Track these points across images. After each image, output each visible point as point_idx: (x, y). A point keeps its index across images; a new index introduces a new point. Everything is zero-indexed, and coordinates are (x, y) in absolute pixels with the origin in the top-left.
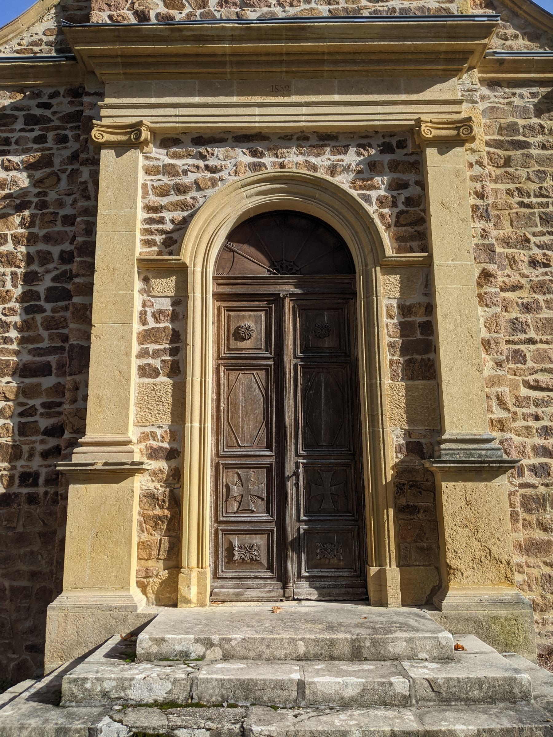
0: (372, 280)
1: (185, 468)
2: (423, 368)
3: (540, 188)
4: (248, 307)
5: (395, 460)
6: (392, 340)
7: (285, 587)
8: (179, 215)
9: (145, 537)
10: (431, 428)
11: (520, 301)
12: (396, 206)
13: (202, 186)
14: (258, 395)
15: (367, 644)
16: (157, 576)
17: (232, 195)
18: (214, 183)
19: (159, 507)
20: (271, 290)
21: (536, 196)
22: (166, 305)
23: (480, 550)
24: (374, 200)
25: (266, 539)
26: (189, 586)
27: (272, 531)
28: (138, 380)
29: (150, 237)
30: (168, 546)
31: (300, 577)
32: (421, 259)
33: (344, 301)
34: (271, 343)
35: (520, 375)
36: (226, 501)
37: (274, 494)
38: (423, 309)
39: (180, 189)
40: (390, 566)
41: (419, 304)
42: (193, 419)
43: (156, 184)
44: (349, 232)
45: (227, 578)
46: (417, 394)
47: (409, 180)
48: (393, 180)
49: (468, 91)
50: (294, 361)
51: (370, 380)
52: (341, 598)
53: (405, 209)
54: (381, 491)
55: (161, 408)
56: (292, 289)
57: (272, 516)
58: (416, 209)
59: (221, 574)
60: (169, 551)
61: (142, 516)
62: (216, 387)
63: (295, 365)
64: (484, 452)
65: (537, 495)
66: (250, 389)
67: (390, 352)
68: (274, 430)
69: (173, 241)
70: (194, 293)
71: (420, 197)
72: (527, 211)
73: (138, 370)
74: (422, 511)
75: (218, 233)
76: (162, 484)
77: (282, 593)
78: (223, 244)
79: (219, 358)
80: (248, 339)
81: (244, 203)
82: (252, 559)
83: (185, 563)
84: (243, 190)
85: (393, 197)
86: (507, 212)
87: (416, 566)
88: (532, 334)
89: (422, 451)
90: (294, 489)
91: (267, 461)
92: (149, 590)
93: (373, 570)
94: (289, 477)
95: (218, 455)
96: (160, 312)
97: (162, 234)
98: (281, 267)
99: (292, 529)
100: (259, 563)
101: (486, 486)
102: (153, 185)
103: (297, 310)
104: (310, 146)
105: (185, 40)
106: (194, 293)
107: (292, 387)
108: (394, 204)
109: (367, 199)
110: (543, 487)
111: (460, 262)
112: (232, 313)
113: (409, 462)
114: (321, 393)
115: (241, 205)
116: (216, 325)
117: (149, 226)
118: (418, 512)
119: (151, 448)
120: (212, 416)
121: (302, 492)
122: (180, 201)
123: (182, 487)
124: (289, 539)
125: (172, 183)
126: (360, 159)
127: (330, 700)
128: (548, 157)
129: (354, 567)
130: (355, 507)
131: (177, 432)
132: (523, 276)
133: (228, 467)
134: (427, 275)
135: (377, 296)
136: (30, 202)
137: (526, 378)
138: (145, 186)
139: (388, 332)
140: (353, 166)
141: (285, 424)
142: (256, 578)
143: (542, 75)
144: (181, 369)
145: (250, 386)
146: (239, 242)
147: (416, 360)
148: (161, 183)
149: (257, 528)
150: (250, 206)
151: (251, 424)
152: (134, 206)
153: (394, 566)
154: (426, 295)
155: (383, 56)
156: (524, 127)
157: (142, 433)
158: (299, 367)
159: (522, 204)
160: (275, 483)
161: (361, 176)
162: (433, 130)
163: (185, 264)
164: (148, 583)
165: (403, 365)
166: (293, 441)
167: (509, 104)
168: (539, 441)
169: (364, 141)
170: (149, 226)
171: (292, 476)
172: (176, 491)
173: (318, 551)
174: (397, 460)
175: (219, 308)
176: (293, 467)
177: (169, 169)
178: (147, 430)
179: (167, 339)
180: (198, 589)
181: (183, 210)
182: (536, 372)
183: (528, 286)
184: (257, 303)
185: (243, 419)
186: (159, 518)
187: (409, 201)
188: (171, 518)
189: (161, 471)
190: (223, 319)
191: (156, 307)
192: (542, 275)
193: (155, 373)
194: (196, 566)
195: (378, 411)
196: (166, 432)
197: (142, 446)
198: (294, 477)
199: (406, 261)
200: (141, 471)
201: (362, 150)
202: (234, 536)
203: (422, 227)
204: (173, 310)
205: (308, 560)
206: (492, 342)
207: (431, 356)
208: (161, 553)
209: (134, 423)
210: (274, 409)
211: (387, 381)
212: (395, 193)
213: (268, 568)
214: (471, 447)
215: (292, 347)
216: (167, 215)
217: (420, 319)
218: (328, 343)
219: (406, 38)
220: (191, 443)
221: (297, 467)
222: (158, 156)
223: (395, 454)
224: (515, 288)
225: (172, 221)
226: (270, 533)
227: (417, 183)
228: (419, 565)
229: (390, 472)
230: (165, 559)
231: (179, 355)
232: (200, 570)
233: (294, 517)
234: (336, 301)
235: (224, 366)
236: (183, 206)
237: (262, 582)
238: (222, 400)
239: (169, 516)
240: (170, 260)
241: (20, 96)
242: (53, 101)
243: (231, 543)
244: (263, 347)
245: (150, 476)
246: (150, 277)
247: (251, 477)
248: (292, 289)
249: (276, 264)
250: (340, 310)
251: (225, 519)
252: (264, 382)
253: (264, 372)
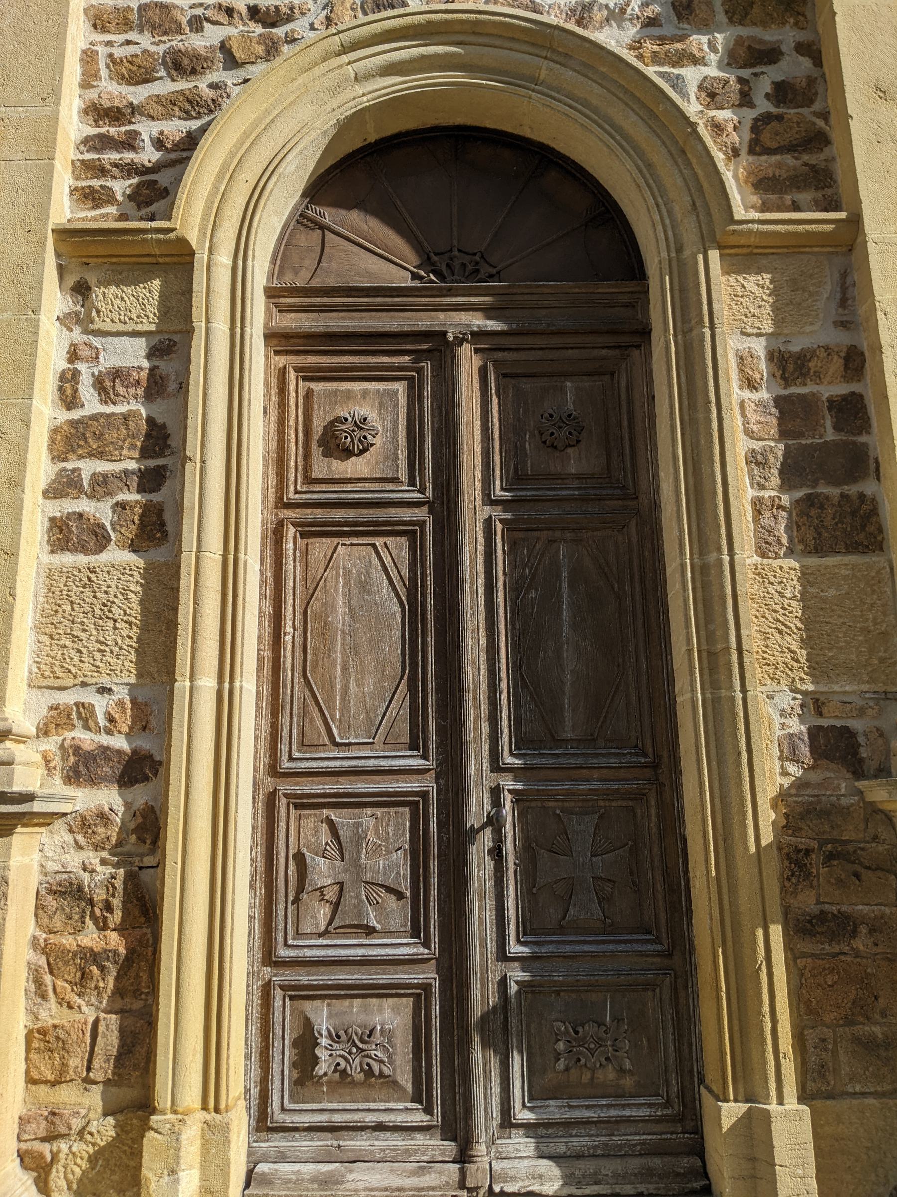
0: (698, 285)
1: (172, 810)
2: (848, 519)
4: (362, 369)
5: (780, 780)
6: (757, 446)
7: (464, 1157)
8: (176, 128)
9: (51, 1014)
10: (879, 687)
12: (751, 105)
13: (239, 55)
14: (388, 602)
16: (81, 1133)
17: (317, 71)
18: (271, 50)
19: (96, 924)
20: (423, 322)
22: (132, 354)
24: (692, 90)
25: (409, 1010)
26: (173, 1172)
27: (426, 987)
28: (46, 558)
29: (96, 183)
30: (116, 1042)
31: (507, 1122)
32: (829, 228)
33: (617, 352)
34: (422, 464)
36: (297, 900)
37: (434, 880)
38: (837, 364)
39: (182, 65)
40: (781, 1102)
41: (827, 348)
42: (199, 666)
43: (118, 53)
44: (629, 164)
45: (296, 1129)
46: (832, 592)
47: (781, 42)
48: (739, 41)
50: (485, 512)
51: (701, 554)
53: (773, 109)
54: (745, 874)
55: (110, 636)
57: (426, 944)
58: (805, 111)
59: (280, 1117)
60: (118, 1058)
61: (44, 952)
62: (271, 581)
63: (489, 523)
66: (365, 587)
67: (752, 478)
68: (432, 697)
69: (155, 191)
70: (208, 320)
71: (811, 81)
73: (50, 529)
74: (863, 929)
75: (280, 169)
76: (105, 854)
77: (456, 1177)
78: (295, 209)
79: (282, 503)
80: (362, 452)
81: (348, 94)
82: (369, 1073)
83: (163, 1096)
84: (345, 58)
85: (740, 80)
87: (854, 1094)
89: (855, 753)
90: (490, 864)
91: (412, 785)
92: (57, 1179)
93: (731, 1112)
94: (475, 831)
95: (273, 770)
96: (116, 373)
97: (129, 176)
98: (447, 264)
99: (485, 981)
100: (390, 1083)
102: (111, 56)
103: (492, 376)
106: (208, 320)
107: (481, 582)
108: (745, 99)
109: (677, 83)
112: (317, 386)
113: (819, 785)
114: (559, 596)
115: (341, 99)
116: (273, 416)
117: (96, 156)
118: (854, 933)
119: (77, 750)
120: (260, 660)
121: (511, 873)
122: (182, 92)
123: (160, 866)
124: (477, 1011)
125: (162, 49)
129: (663, 1091)
130: (662, 916)
131: (152, 709)
133: (301, 803)
134: (844, 275)
135: (712, 327)
138: (88, 57)
139: (746, 423)
141: (461, 681)
142: (380, 1127)
144: (170, 528)
145: (365, 578)
146: (338, 204)
147: (827, 498)
148: (132, 50)
149: (383, 977)
150: (365, 102)
151: (369, 681)
152: (52, 95)
153: (792, 1103)
154: (843, 325)
157: (51, 708)
158: (499, 526)
160: (434, 850)
161: (656, 31)
163: (183, 242)
164: (55, 1156)
165: (790, 514)
166: (485, 727)
170: (96, 156)
171: (482, 828)
172: (145, 876)
173: (561, 1046)
174: (786, 782)
175: (282, 372)
176: (487, 801)
177: (155, 16)
178: (68, 698)
179: (132, 447)
180: (204, 1178)
181: (188, 117)
184: (385, 359)
185: (345, 668)
186: (94, 957)
187: (782, 92)
188: (127, 958)
189: (103, 818)
190: (292, 401)
191: (106, 362)
193: (98, 539)
194: (198, 1104)
195: (727, 640)
196: (120, 704)
197: (51, 744)
198: (488, 831)
199: (789, 234)
200: (47, 819)
202: (318, 1003)
203: (822, 156)
204: (152, 370)
205: (532, 1072)
207: (868, 487)
208: (96, 1064)
209: (30, 680)
210: (431, 640)
211: (747, 556)
212: (746, 73)
213: (416, 1099)
215: (478, 474)
216: (146, 129)
217: (831, 388)
218: (575, 462)
220: (190, 736)
221: (497, 803)
223: (778, 763)
225: (159, 143)
226: (420, 995)
227: (803, 49)
228: (863, 1094)
229: (768, 817)
230: (107, 1083)
231: (165, 490)
232: (210, 1116)
233: (491, 946)
234: (595, 352)
235: (294, 525)
236: (192, 106)
237: (396, 1141)
238: (289, 616)
239: (122, 950)
240: (145, 231)
243: (308, 1024)
245: (71, 831)
246: (92, 280)
247: (366, 831)
248: (478, 321)
249: (435, 258)
250: (607, 378)
251: (292, 953)
252: (405, 570)
253: (403, 541)
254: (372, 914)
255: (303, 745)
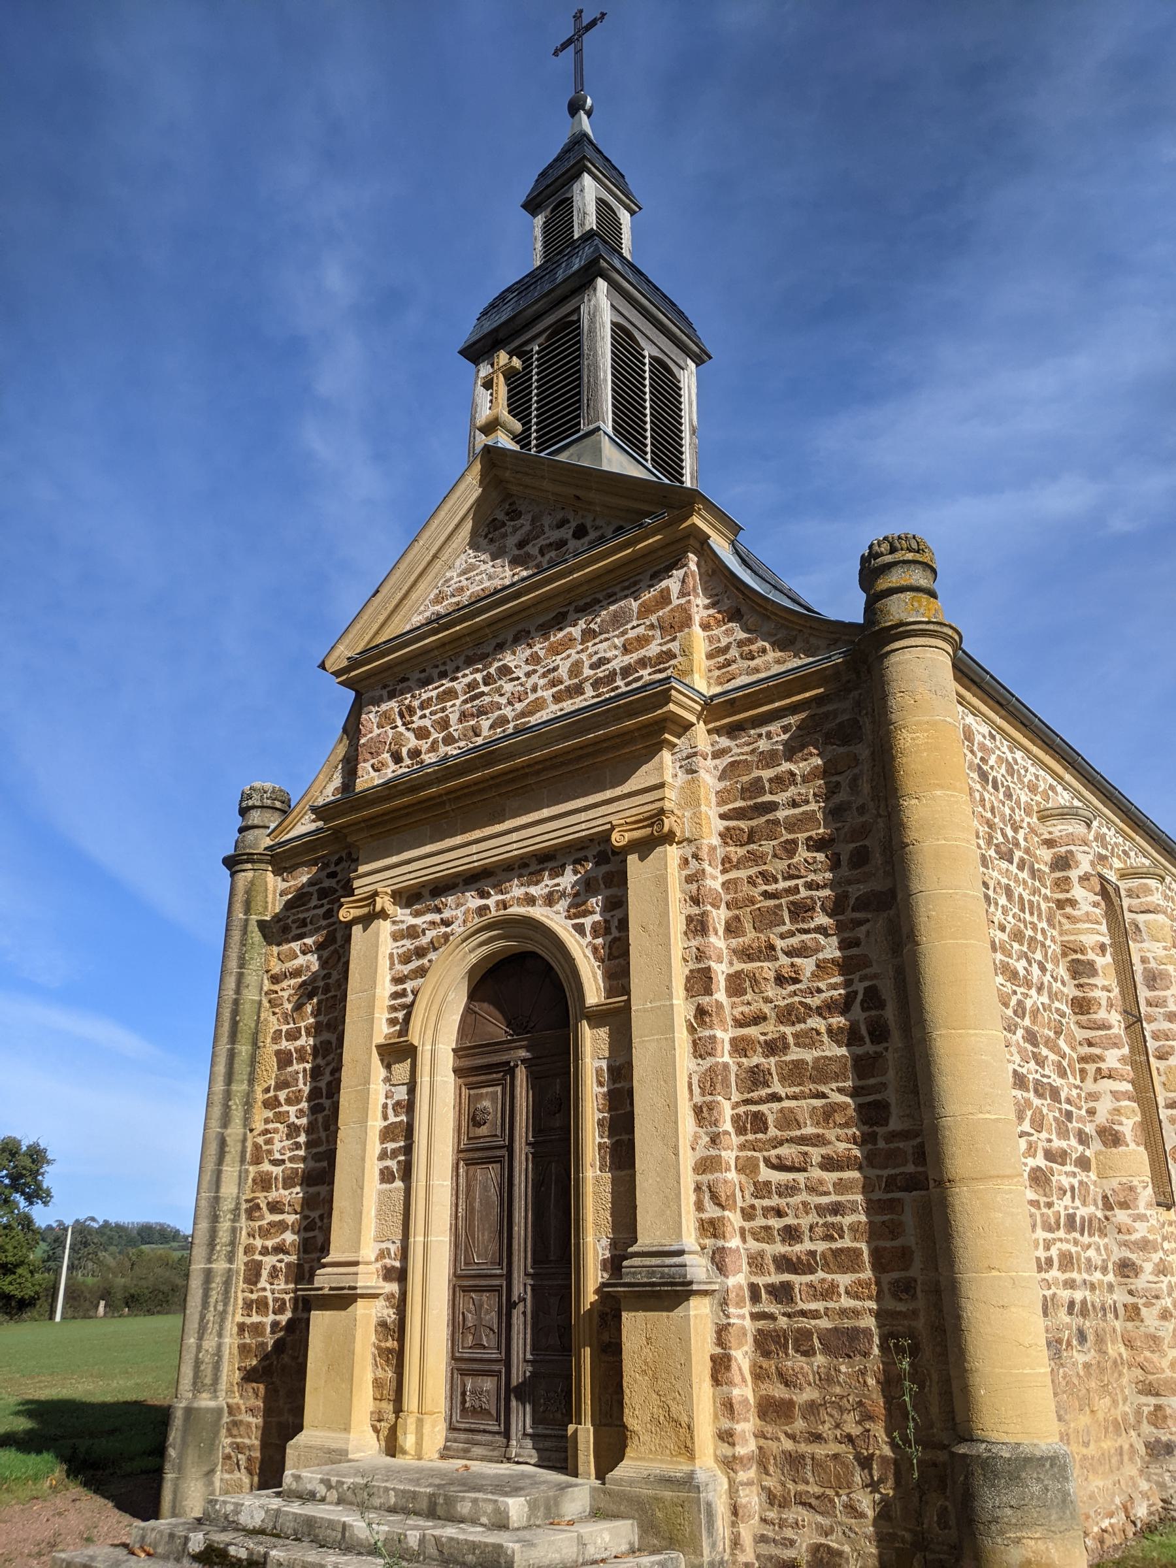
3: (789, 866)
9: (380, 1373)
11: (762, 1038)
15: (441, 1501)
21: (785, 879)
23: (659, 1406)
35: (761, 1151)
49: (688, 758)
52: (559, 1465)
56: (523, 1053)
64: (666, 1269)
65: (775, 1331)
72: (771, 903)
86: (748, 909)
88: (777, 1087)
91: (497, 1282)
101: (668, 1317)
104: (530, 874)
105: (402, 794)
110: (785, 1319)
111: (658, 1004)
125: (412, 947)
126: (575, 878)
127: (361, 1545)
128: (800, 817)
132: (767, 1000)
136: (318, 987)
137: (766, 1154)
140: (569, 890)
142: (485, 1431)
143: (788, 701)
148: (404, 949)
149: (487, 1367)
150: (474, 961)
155: (580, 752)
156: (770, 780)
159: (766, 895)
162: (626, 834)
163: (412, 1044)
167: (753, 751)
168: (780, 1248)
169: (580, 855)
182: (781, 1145)
183: (774, 1015)
192: (790, 996)
197: (379, 1265)
201: (579, 867)
205: (534, 1412)
206: (705, 1109)
214: (648, 1263)
219: (589, 731)
222: (403, 918)
224: (758, 1019)
237: (489, 1438)
241: (315, 869)
242: (338, 869)
244: (498, 1133)
254: (484, 1338)
255: (466, 1264)
